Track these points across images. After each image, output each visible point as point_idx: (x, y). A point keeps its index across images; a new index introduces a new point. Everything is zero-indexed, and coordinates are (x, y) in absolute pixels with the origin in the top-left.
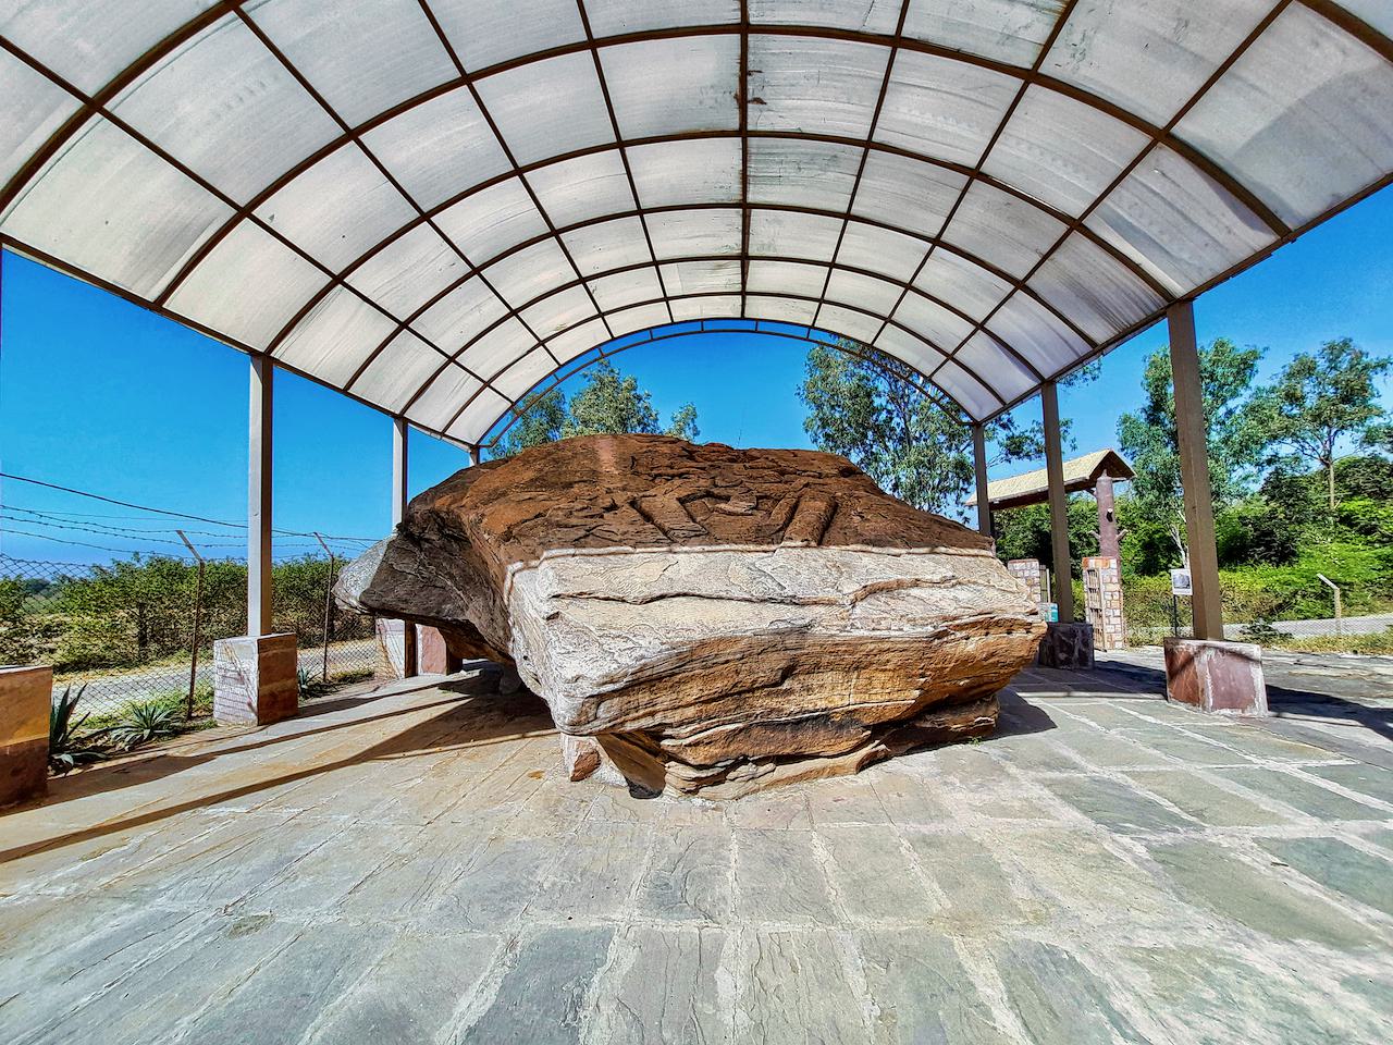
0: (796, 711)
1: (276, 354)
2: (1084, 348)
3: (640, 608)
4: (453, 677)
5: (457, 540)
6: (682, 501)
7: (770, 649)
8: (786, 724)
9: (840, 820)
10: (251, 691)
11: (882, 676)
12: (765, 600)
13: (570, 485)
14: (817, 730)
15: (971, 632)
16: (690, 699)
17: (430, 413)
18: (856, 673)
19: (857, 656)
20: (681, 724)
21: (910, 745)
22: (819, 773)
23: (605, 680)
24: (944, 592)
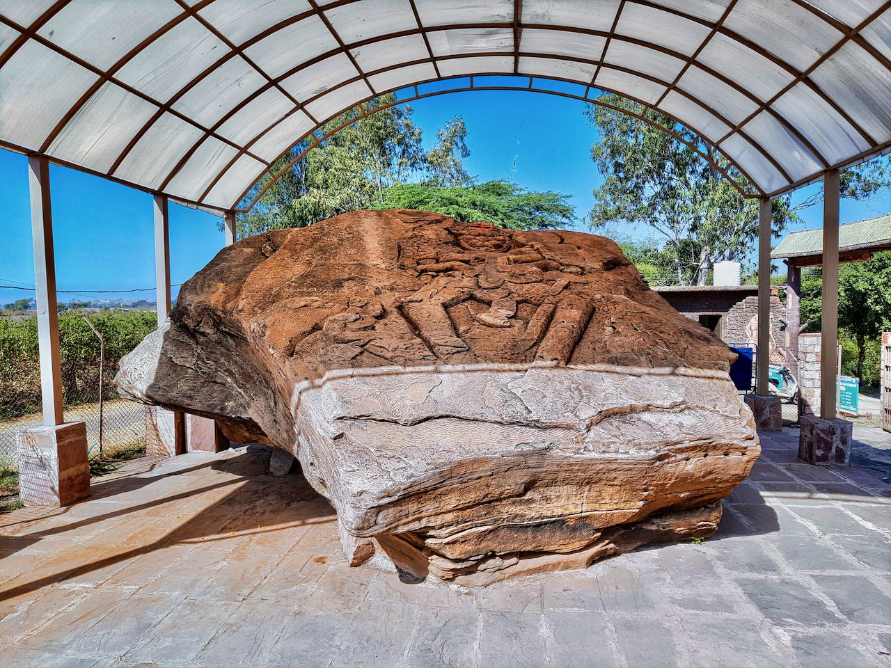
0: (536, 517)
1: (48, 153)
2: (865, 146)
3: (409, 428)
4: (223, 455)
5: (232, 336)
7: (515, 468)
8: (527, 527)
9: (564, 606)
10: (53, 475)
11: (610, 490)
12: (514, 423)
13: (339, 284)
14: (554, 532)
15: (691, 454)
16: (450, 507)
17: (187, 186)
18: (588, 487)
19: (589, 474)
20: (441, 527)
21: (639, 544)
22: (555, 566)
23: (384, 494)
24: (672, 417)
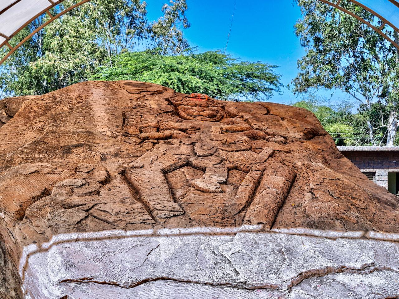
3: (129, 291)
6: (165, 172)
13: (68, 150)
